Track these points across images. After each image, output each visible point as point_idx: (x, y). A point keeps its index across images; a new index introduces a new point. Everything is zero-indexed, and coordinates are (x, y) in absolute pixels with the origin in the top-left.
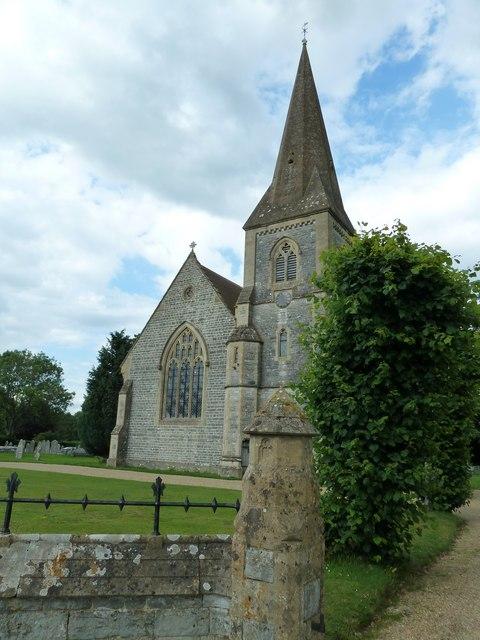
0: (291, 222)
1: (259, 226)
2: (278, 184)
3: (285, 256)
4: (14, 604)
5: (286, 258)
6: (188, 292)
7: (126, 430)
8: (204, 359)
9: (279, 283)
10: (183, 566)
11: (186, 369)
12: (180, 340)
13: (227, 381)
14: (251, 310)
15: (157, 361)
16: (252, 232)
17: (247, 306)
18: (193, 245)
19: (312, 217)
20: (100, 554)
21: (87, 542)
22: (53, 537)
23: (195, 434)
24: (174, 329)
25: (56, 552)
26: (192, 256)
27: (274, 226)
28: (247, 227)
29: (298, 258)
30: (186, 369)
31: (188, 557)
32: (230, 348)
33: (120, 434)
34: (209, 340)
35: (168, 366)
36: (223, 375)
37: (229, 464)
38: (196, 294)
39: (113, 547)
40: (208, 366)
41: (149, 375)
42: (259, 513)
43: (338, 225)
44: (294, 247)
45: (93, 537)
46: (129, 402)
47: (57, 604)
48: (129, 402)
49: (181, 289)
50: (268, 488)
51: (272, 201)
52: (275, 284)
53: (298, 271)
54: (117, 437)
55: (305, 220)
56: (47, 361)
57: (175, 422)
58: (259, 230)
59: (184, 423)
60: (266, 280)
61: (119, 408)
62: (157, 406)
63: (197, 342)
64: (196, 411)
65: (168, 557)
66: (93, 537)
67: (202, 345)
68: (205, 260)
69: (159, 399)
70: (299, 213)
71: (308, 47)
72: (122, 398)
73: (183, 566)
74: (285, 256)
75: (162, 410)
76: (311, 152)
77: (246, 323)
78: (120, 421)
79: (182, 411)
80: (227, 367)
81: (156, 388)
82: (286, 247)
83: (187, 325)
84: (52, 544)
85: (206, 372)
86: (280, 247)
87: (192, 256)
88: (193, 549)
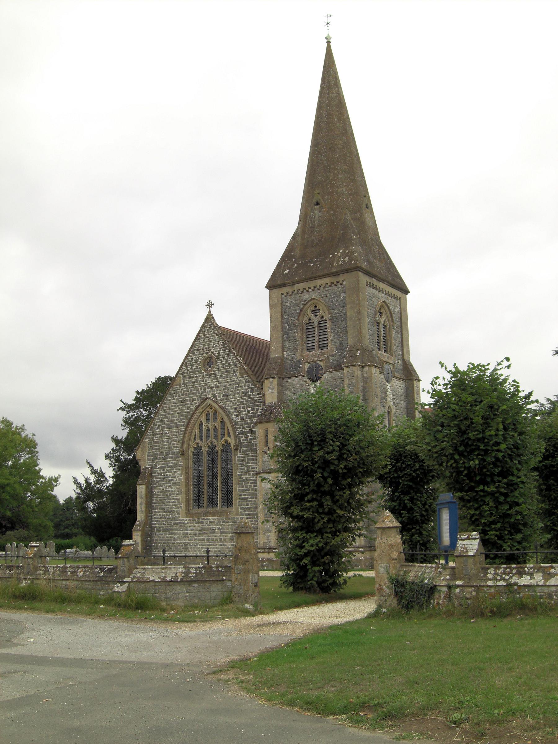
0: (319, 282)
1: (283, 285)
2: (304, 232)
3: (315, 320)
4: (171, 583)
5: (316, 323)
6: (209, 361)
7: (149, 524)
8: (232, 441)
9: (310, 353)
10: (217, 573)
11: (212, 451)
12: (204, 421)
13: (259, 467)
14: (279, 385)
15: (178, 444)
16: (276, 291)
17: (275, 382)
18: (210, 305)
19: (341, 278)
20: (192, 571)
21: (188, 568)
22: (178, 566)
23: (228, 526)
24: (194, 407)
25: (180, 570)
26: (210, 319)
27: (301, 286)
28: (271, 286)
29: (329, 324)
30: (212, 451)
31: (218, 571)
32: (260, 430)
33: (143, 531)
34: (236, 420)
35: (191, 450)
36: (254, 459)
37: (266, 556)
38: (218, 366)
39: (196, 568)
40: (236, 449)
41: (169, 462)
42: (238, 555)
43: (375, 281)
44: (324, 312)
45: (189, 566)
46: (150, 493)
47: (183, 583)
48: (150, 493)
49: (200, 359)
50: (240, 548)
51: (297, 252)
52: (305, 353)
53: (330, 339)
54: (139, 533)
55: (334, 279)
56: (17, 432)
57: (205, 514)
58: (285, 290)
59: (213, 514)
60: (295, 350)
61: (139, 501)
62: (182, 497)
63: (222, 422)
64: (228, 501)
65: (213, 571)
66: (189, 566)
67: (228, 425)
68: (222, 321)
69: (184, 489)
70: (326, 271)
71: (332, 45)
72: (141, 489)
73: (217, 573)
74: (315, 320)
75: (188, 501)
76: (339, 190)
77: (275, 400)
78: (140, 516)
79: (212, 502)
80: (258, 452)
81: (179, 476)
82: (315, 311)
83: (209, 401)
84: (178, 568)
85: (235, 457)
86: (309, 312)
87: (210, 319)
88: (220, 569)
